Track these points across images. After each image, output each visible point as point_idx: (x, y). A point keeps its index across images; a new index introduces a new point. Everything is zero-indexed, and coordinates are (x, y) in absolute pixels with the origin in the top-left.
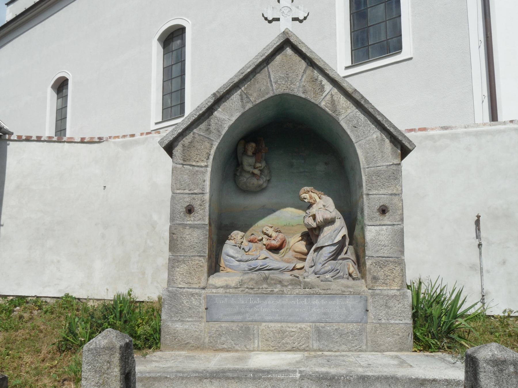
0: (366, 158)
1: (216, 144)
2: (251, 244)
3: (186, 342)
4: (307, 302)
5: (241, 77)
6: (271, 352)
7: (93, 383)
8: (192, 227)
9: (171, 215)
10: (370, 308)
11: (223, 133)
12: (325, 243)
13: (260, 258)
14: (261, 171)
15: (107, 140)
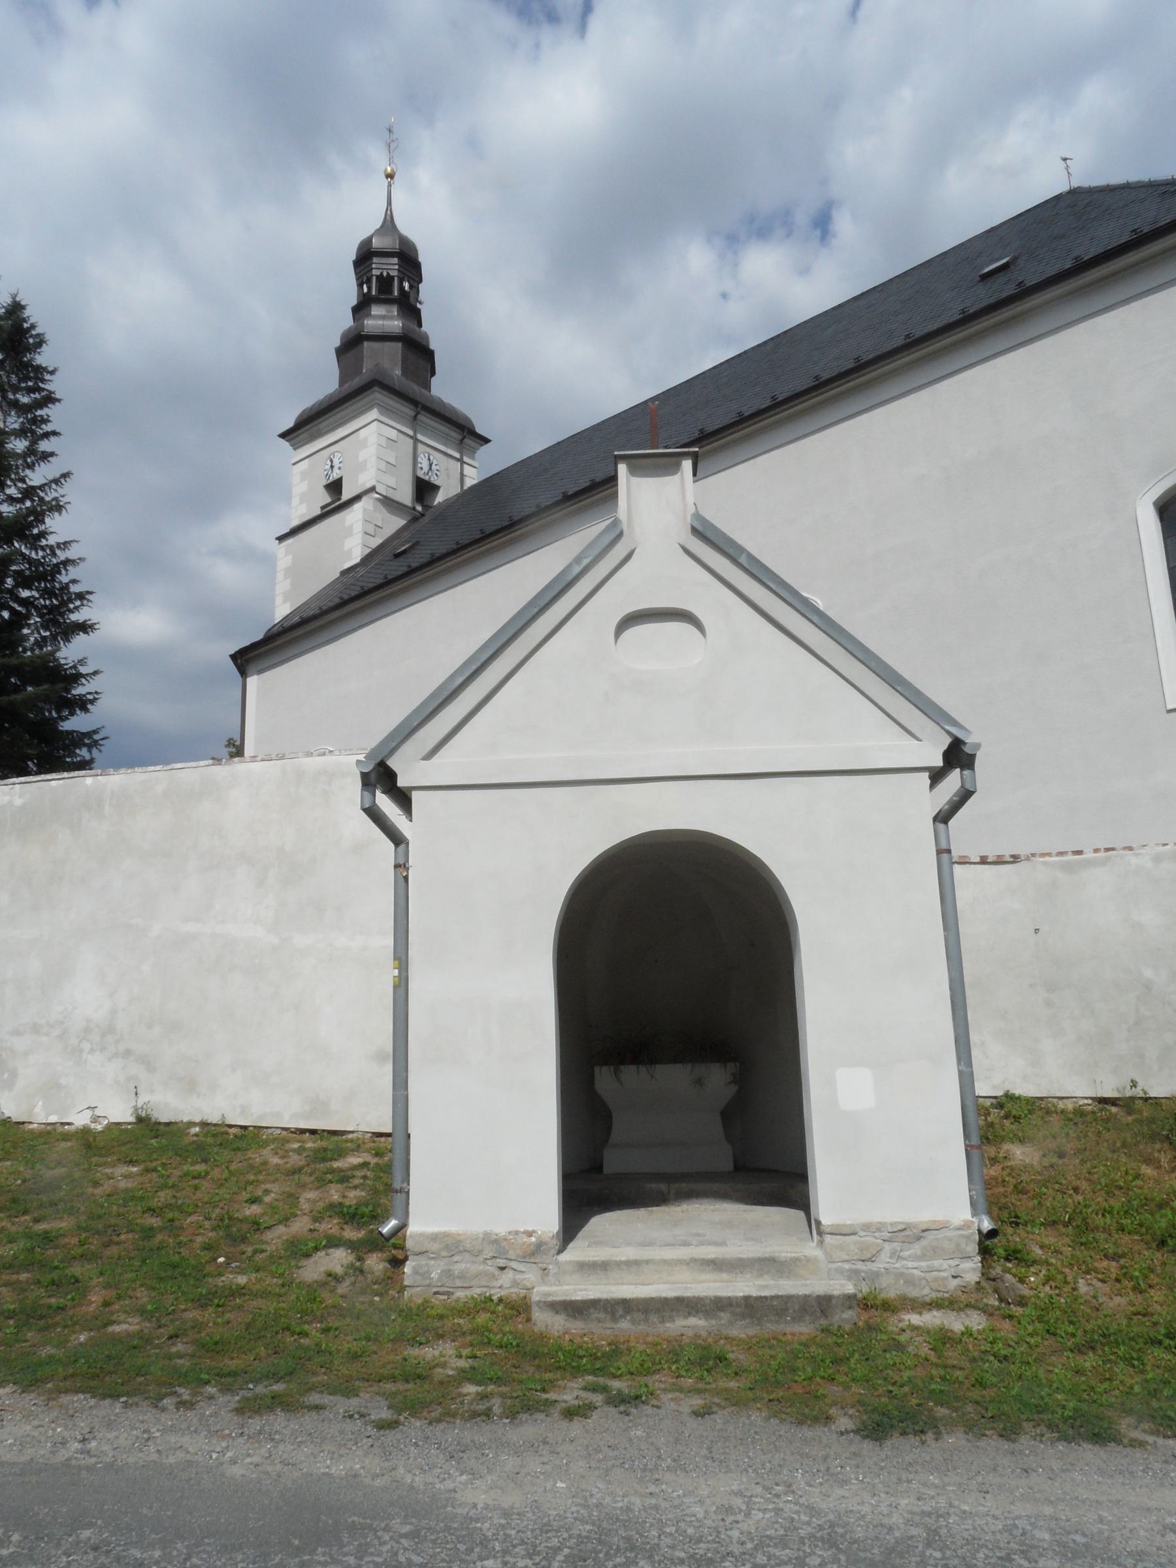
15: (1027, 859)
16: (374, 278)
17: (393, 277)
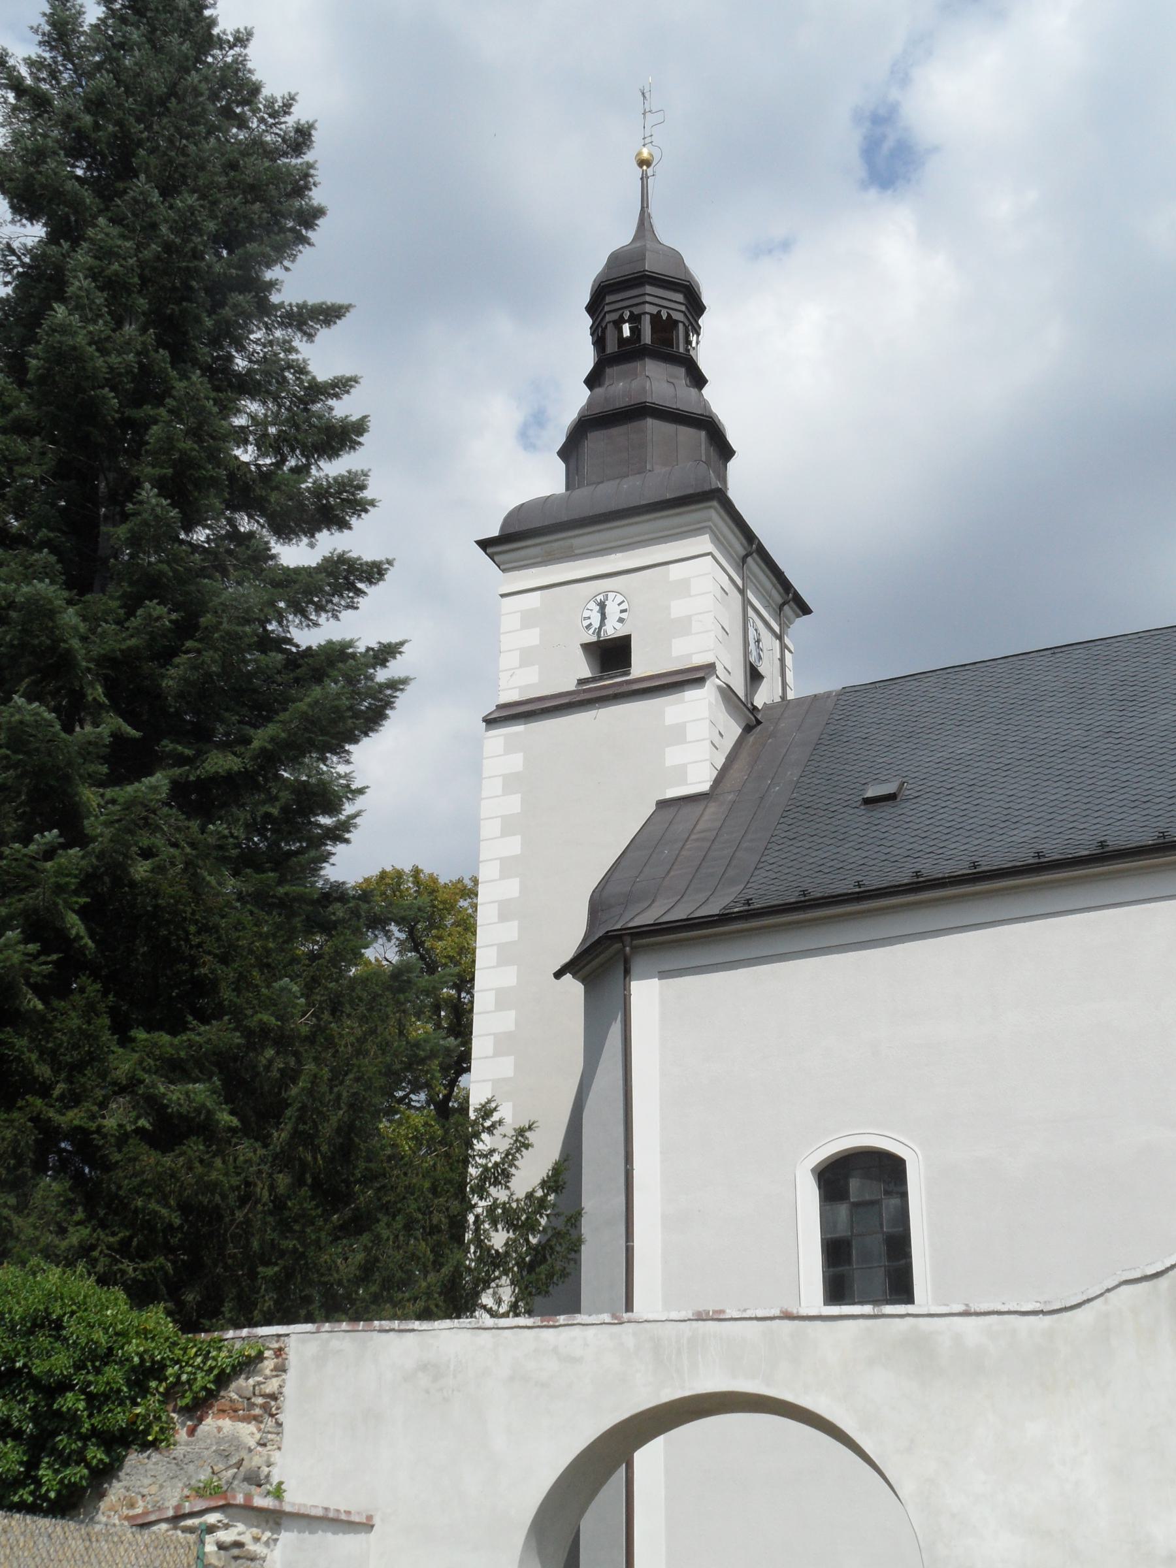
16: (648, 317)
17: (676, 322)
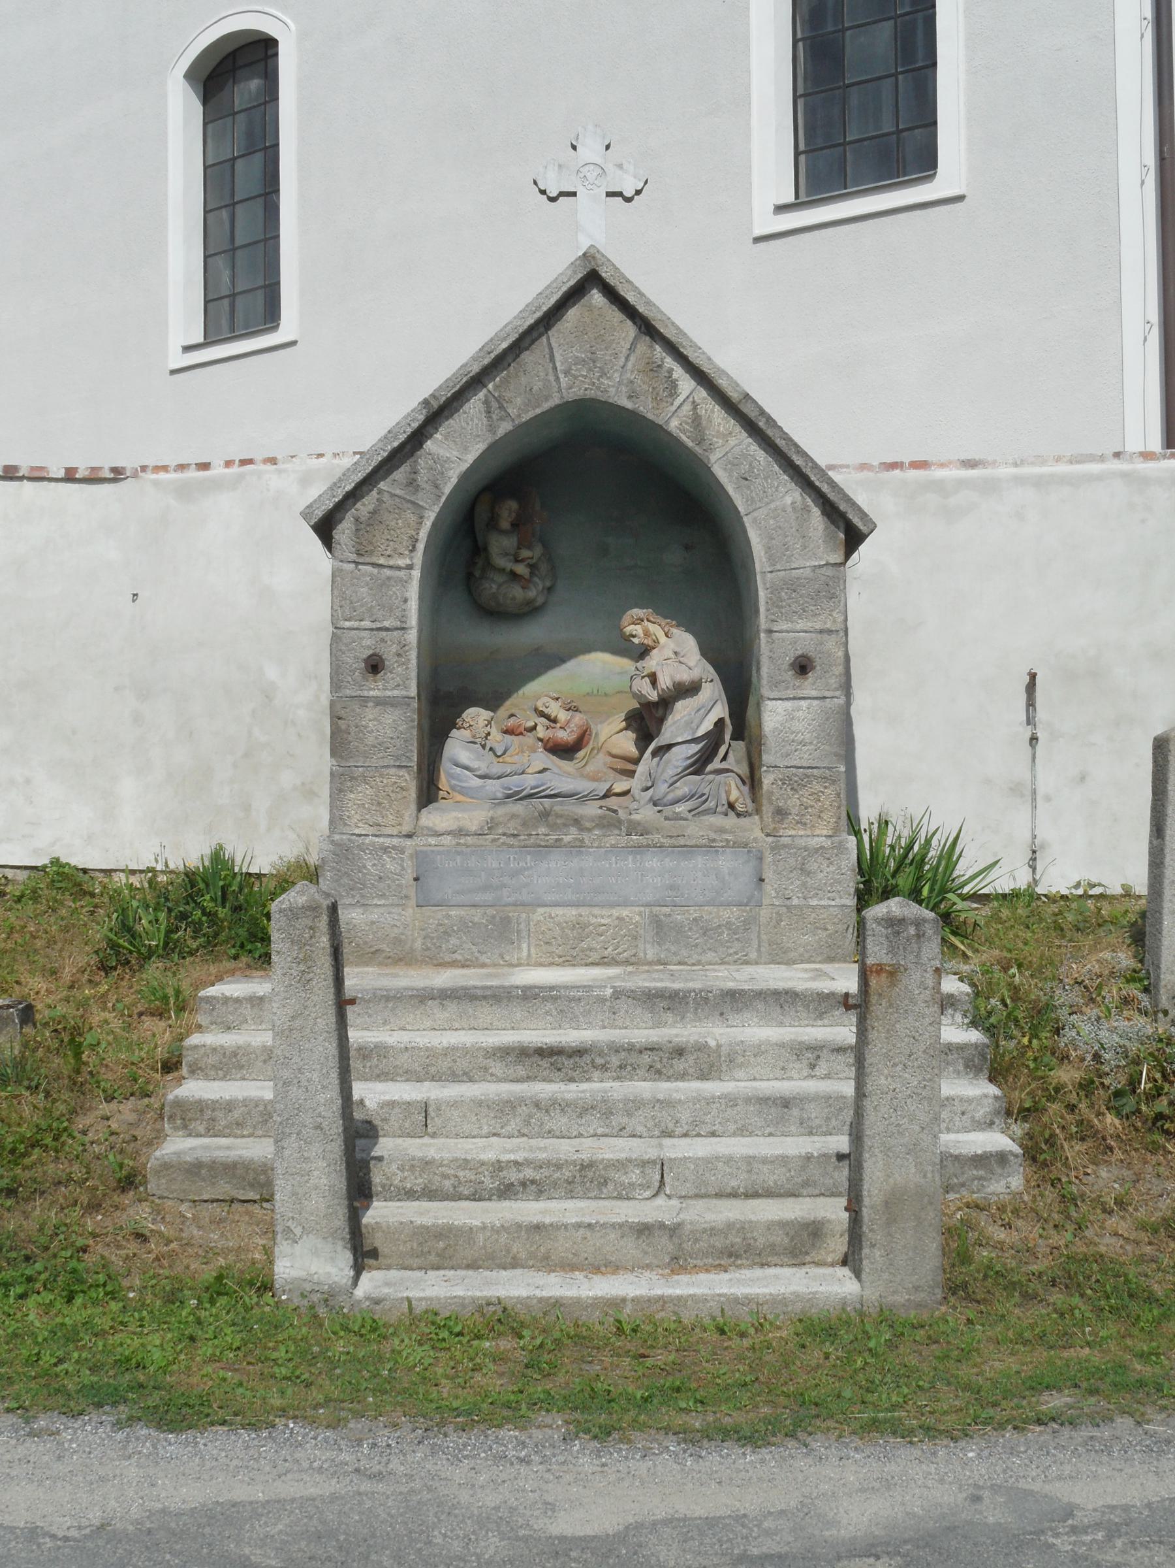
0: (768, 549)
1: (430, 517)
2: (508, 737)
3: (373, 950)
4: (634, 862)
5: (486, 361)
6: (555, 968)
7: (289, 959)
8: (380, 702)
9: (331, 678)
10: (768, 875)
11: (447, 490)
12: (677, 736)
13: (530, 770)
14: (533, 567)
15: (135, 476)
